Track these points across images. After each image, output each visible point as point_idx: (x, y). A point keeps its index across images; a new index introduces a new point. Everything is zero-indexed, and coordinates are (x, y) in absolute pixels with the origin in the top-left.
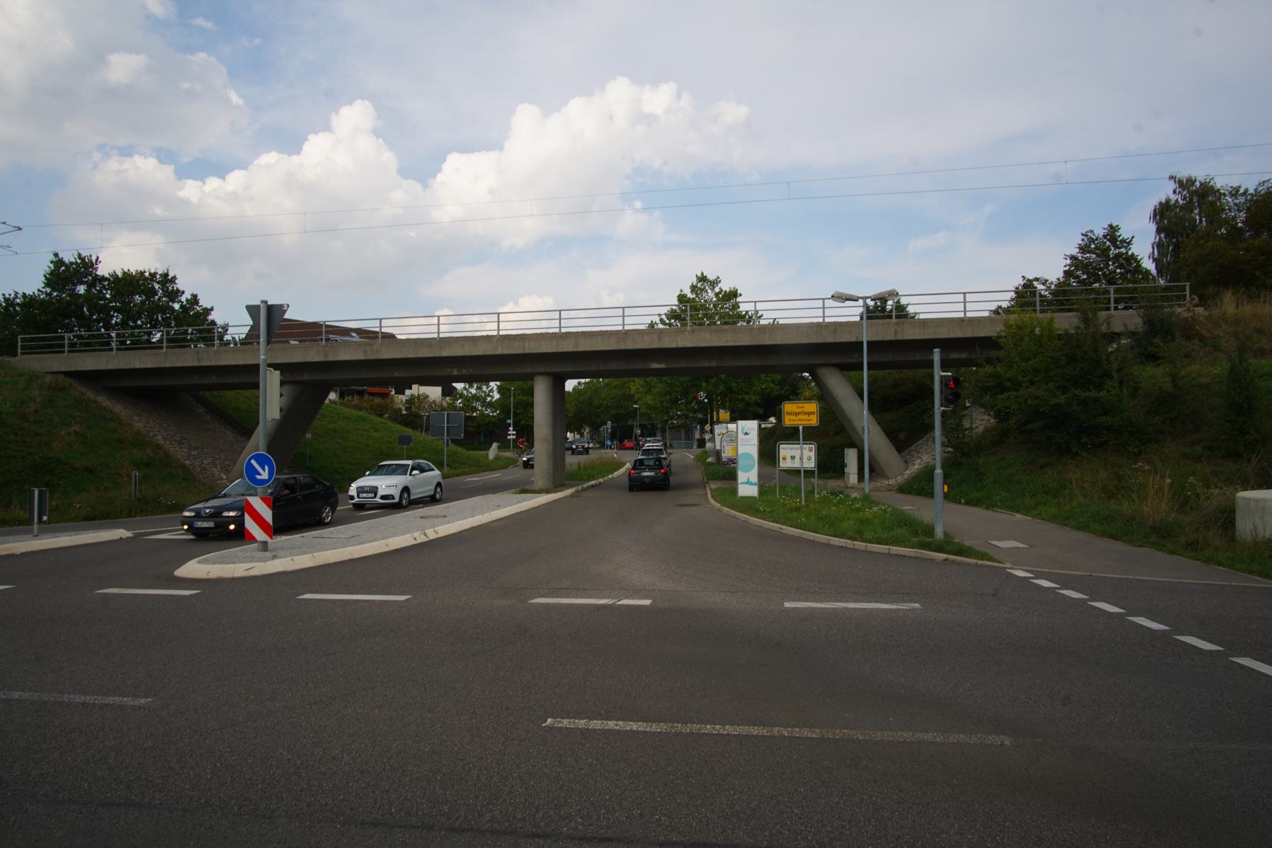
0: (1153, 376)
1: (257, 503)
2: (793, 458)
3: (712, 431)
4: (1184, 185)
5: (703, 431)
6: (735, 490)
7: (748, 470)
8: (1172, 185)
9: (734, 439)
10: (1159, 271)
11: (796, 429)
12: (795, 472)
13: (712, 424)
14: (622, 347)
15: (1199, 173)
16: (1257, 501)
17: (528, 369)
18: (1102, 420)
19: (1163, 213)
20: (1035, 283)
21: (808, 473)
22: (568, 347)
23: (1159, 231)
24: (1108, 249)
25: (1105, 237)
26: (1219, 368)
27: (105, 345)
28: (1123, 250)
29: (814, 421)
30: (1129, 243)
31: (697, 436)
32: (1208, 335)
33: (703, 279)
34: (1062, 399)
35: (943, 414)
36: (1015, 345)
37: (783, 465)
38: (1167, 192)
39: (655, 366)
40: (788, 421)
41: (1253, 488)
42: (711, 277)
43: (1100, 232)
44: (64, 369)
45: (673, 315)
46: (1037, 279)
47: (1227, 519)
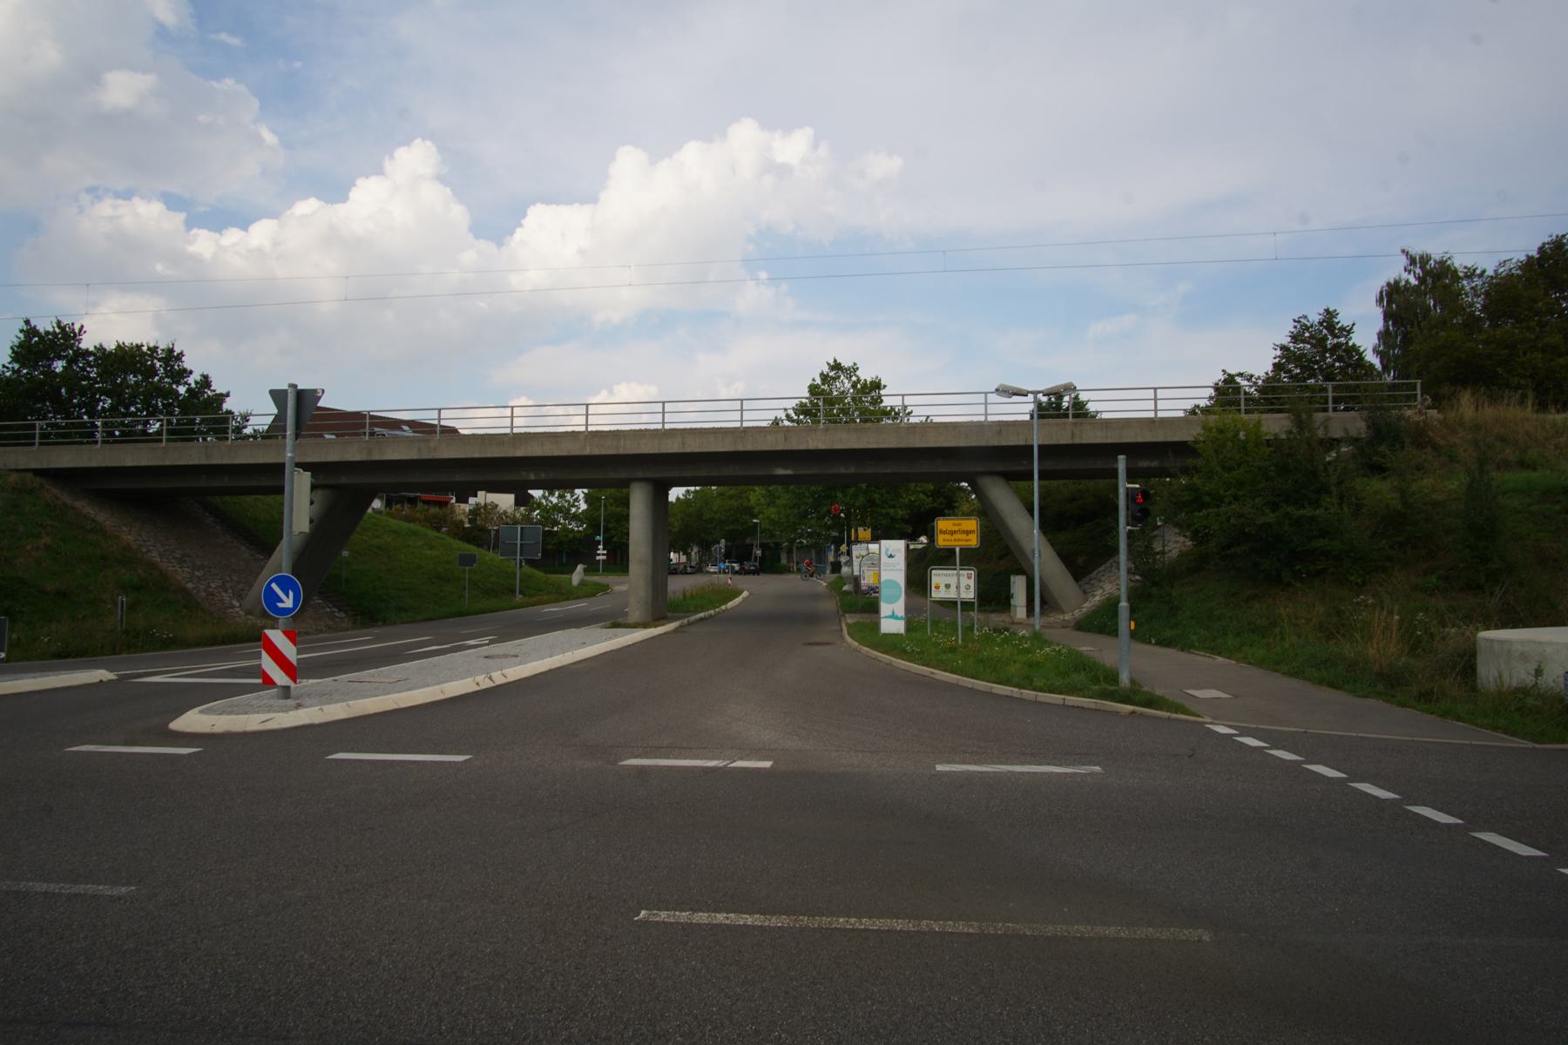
0: (1380, 491)
1: (277, 637)
2: (948, 586)
3: (849, 553)
4: (1416, 261)
5: (838, 553)
6: (877, 625)
7: (892, 601)
8: (1404, 261)
9: (876, 563)
10: (1385, 367)
11: (951, 551)
12: (950, 604)
13: (850, 543)
14: (740, 448)
15: (1436, 250)
16: (1501, 642)
17: (623, 475)
18: (1319, 543)
19: (1394, 298)
20: (1238, 379)
21: (967, 605)
22: (673, 447)
23: (1387, 316)
24: (1325, 339)
25: (1321, 323)
26: (1456, 483)
27: (88, 435)
28: (1342, 340)
29: (973, 541)
30: (1349, 332)
31: (831, 558)
32: (1442, 443)
33: (836, 366)
34: (1271, 518)
35: (1130, 534)
36: (1216, 451)
37: (936, 595)
38: (1396, 270)
39: (780, 472)
40: (942, 541)
41: (1497, 627)
42: (846, 363)
43: (1315, 317)
44: (34, 466)
45: (802, 410)
46: (1240, 375)
47: (1466, 665)
